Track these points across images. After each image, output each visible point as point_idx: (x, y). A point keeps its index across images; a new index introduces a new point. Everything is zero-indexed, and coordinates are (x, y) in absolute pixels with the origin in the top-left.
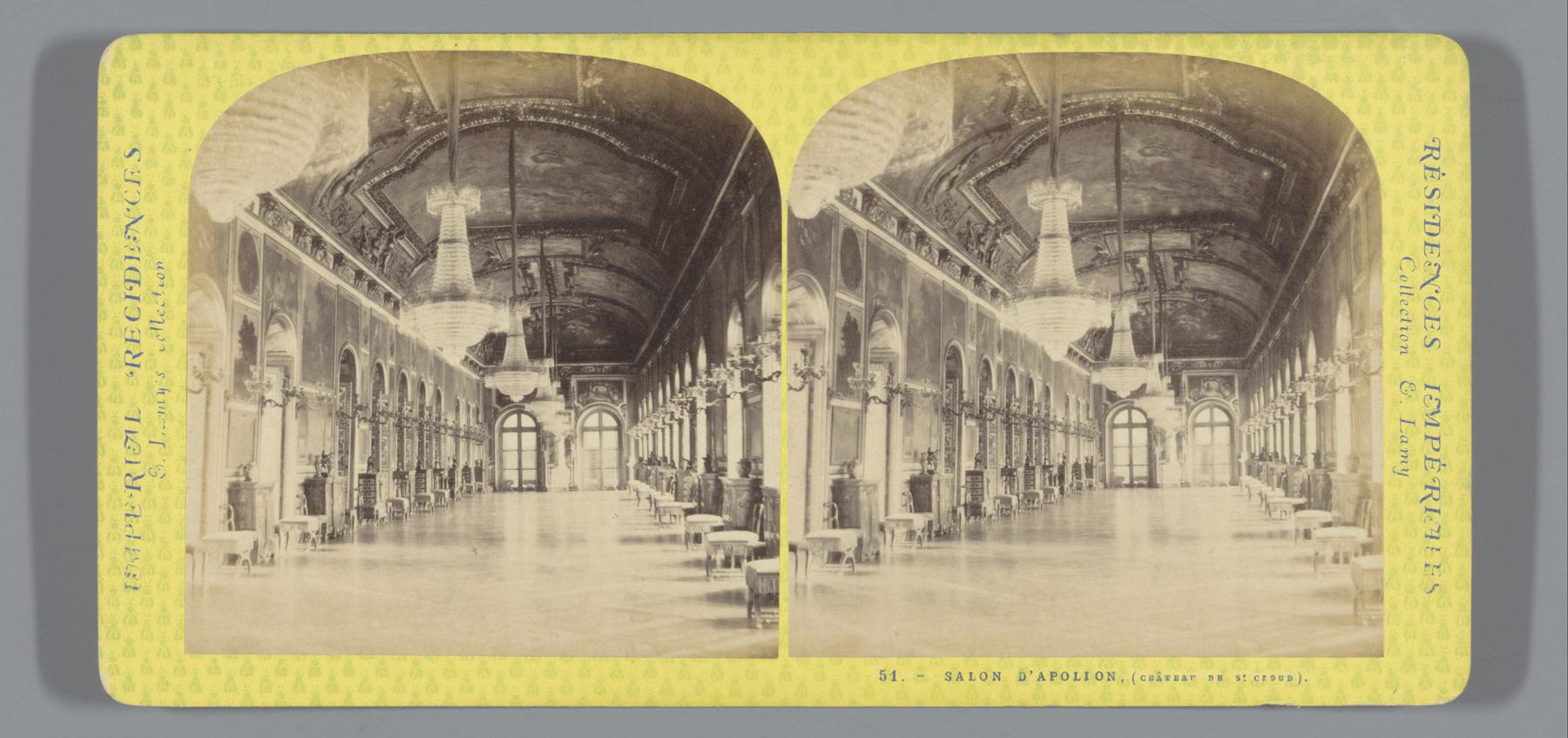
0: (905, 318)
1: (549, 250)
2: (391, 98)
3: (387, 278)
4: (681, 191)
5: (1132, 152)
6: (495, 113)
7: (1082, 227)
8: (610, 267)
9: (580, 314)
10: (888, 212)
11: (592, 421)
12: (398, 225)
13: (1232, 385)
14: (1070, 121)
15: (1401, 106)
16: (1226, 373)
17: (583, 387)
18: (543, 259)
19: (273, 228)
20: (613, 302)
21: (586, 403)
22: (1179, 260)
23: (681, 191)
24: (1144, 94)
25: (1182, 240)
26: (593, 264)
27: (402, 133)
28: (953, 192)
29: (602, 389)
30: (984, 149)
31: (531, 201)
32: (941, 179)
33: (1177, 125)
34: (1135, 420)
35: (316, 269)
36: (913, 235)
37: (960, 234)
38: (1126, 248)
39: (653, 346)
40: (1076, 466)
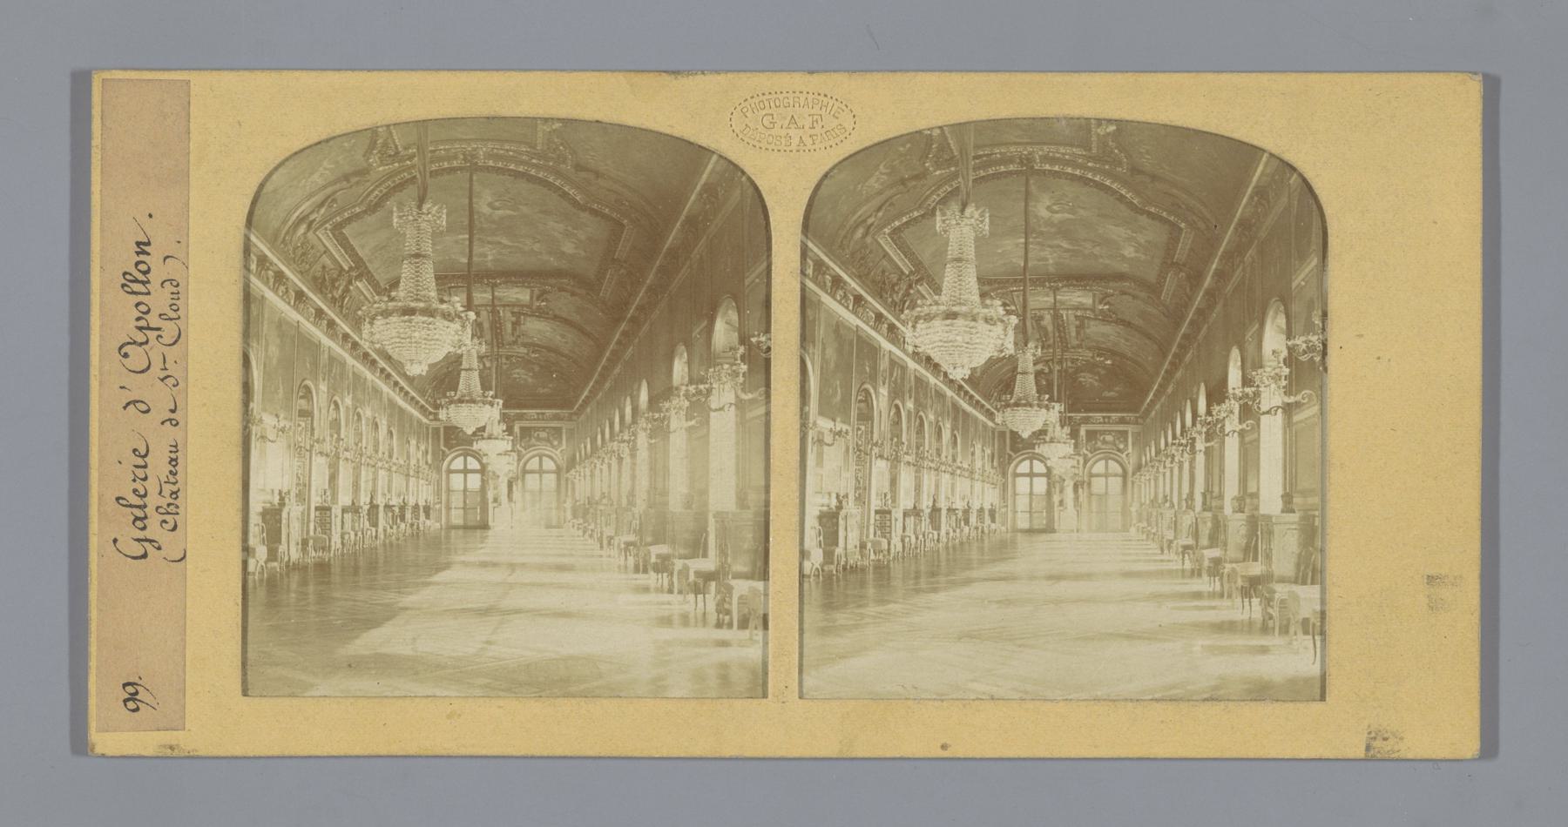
1: (1062, 303)
5: (1042, 208)
7: (990, 282)
8: (556, 317)
9: (1091, 367)
12: (918, 271)
13: (1126, 440)
14: (491, 163)
15: (1391, 169)
16: (1121, 428)
20: (556, 351)
21: (1094, 450)
22: (517, 315)
24: (1053, 148)
25: (521, 295)
26: (541, 314)
29: (543, 435)
31: (1046, 253)
32: (301, 220)
33: (1083, 180)
34: (1036, 470)
37: (315, 279)
39: (600, 383)
40: (981, 510)
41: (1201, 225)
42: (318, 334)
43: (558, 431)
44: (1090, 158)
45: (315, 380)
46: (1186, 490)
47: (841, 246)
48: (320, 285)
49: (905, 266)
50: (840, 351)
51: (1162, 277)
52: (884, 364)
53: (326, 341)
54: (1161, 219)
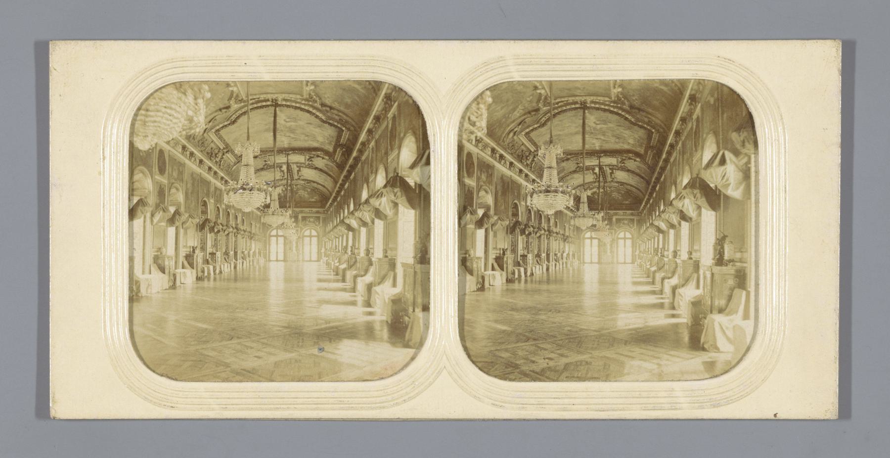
0: (494, 191)
2: (532, 95)
3: (533, 172)
4: (655, 137)
6: (268, 100)
10: (486, 146)
11: (307, 233)
16: (632, 217)
17: (304, 218)
18: (601, 168)
19: (173, 147)
21: (305, 225)
22: (612, 169)
23: (655, 137)
25: (613, 161)
26: (311, 167)
27: (537, 110)
28: (515, 137)
30: (528, 120)
31: (594, 141)
35: (192, 166)
36: (498, 155)
38: (277, 161)
39: (646, 204)
41: (352, 128)
42: (210, 178)
43: (318, 218)
44: (611, 102)
45: (519, 200)
46: (344, 244)
47: (503, 141)
48: (210, 155)
49: (222, 146)
50: (193, 185)
51: (335, 151)
52: (212, 189)
53: (213, 180)
54: (334, 126)
